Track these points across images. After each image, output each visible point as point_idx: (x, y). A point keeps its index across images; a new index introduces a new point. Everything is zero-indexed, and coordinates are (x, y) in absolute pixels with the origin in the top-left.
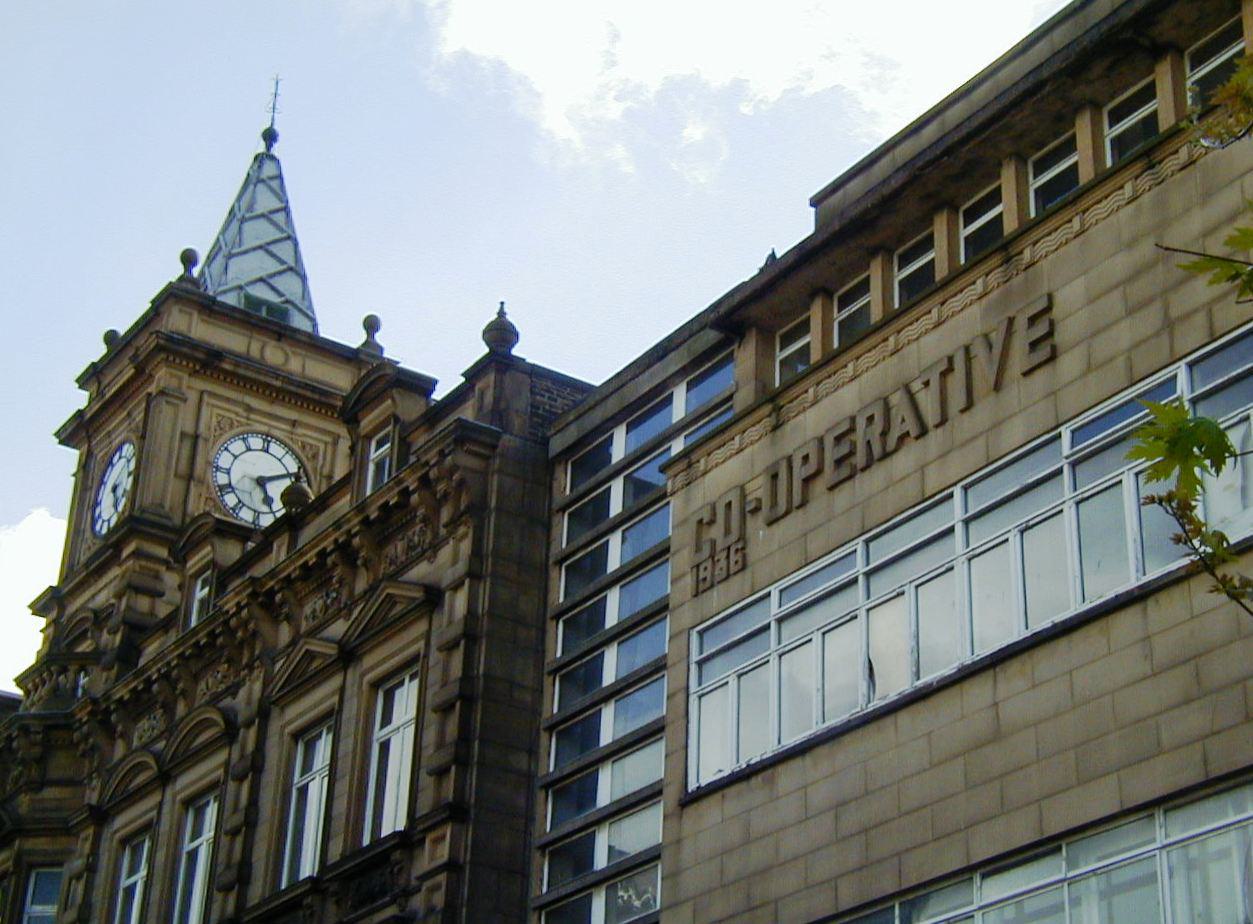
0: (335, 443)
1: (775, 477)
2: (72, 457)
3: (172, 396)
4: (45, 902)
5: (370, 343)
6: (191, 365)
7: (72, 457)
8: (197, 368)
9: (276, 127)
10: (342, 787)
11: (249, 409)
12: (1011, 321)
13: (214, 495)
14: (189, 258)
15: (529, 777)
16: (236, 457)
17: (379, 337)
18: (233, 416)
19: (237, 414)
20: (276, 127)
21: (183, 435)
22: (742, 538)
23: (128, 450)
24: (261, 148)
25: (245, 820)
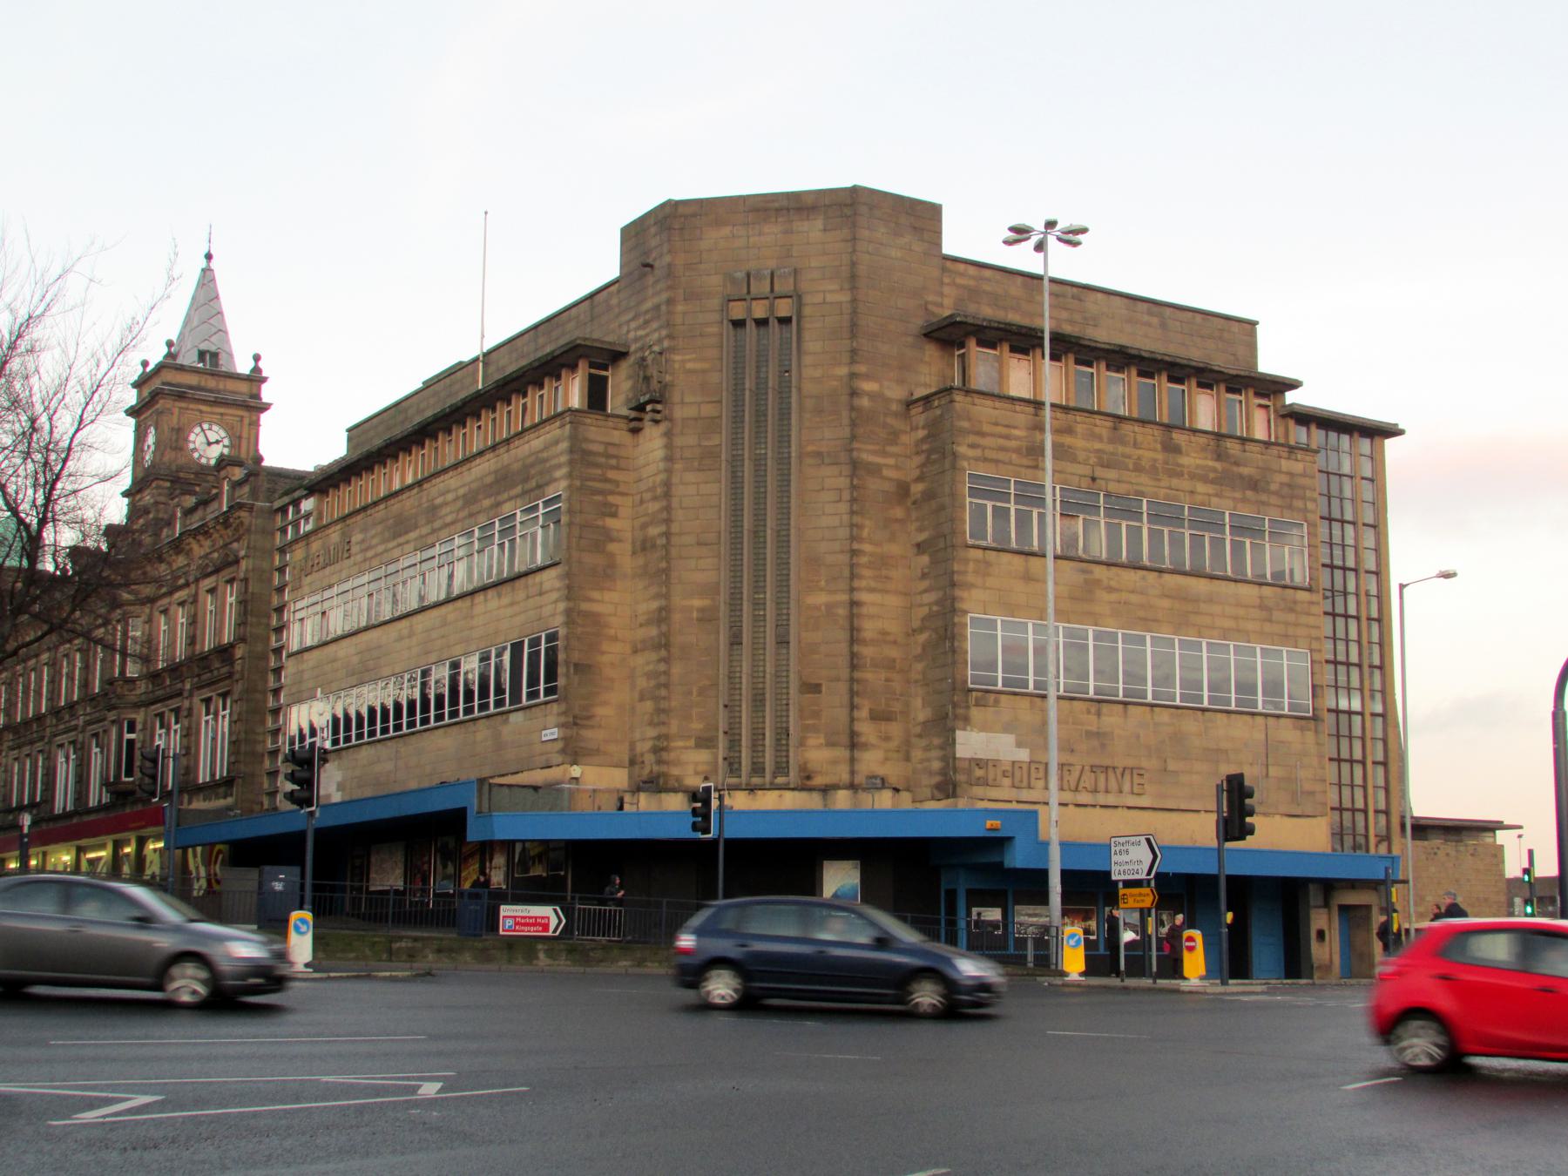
0: (242, 421)
4: (136, 631)
5: (257, 370)
9: (212, 252)
10: (218, 617)
11: (201, 412)
15: (268, 625)
21: (173, 429)
23: (152, 430)
25: (821, 793)
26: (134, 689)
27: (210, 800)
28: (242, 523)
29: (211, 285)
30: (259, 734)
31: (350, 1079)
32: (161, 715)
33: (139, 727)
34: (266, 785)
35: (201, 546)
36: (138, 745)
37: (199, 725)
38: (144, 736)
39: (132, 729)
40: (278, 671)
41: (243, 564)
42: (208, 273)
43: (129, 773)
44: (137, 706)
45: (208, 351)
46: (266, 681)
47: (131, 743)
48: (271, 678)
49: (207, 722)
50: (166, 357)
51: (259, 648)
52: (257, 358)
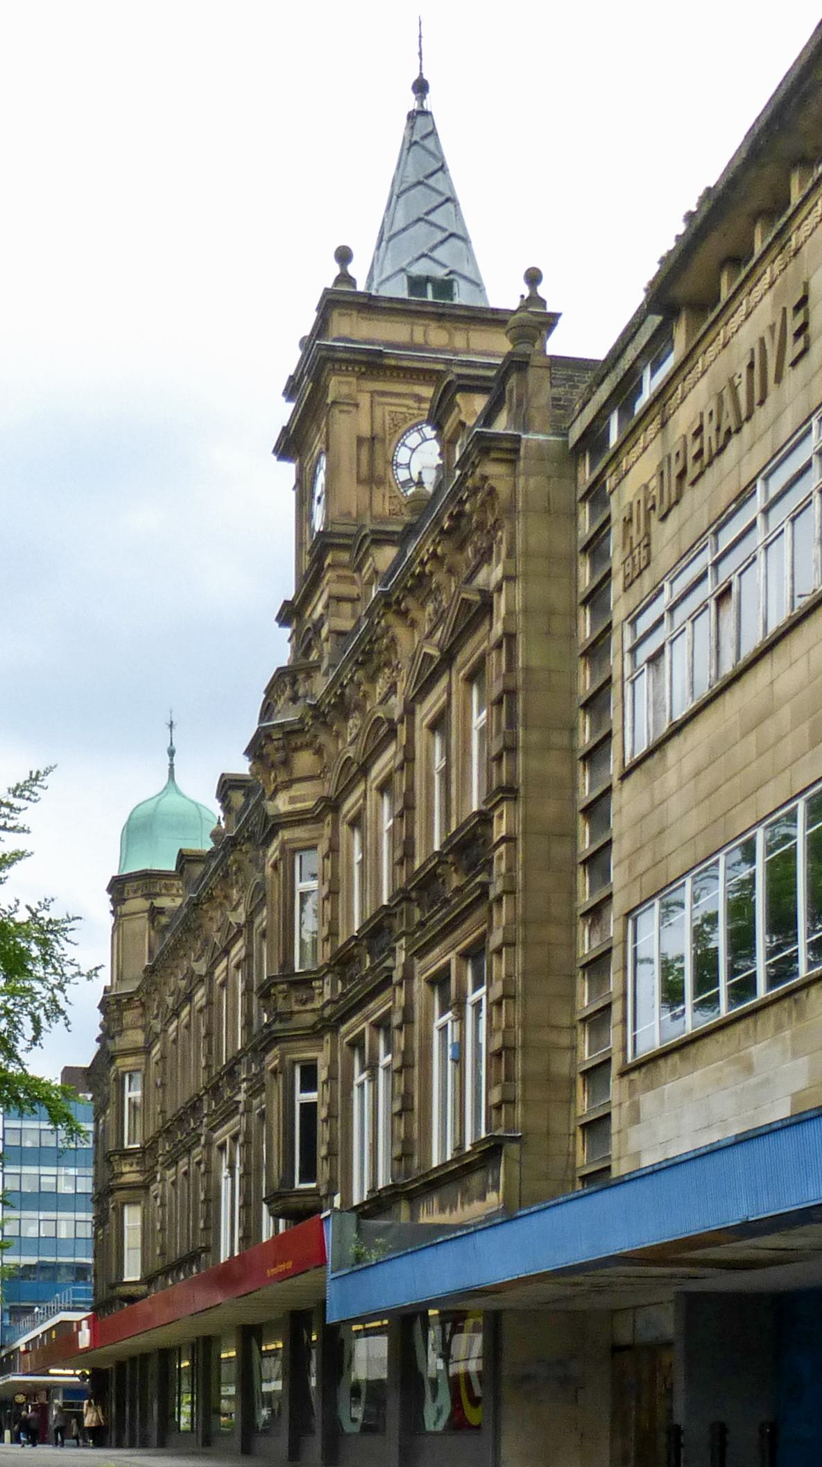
1: (662, 474)
2: (288, 470)
3: (343, 403)
5: (534, 300)
6: (357, 369)
7: (288, 470)
8: (363, 370)
12: (785, 309)
13: (397, 493)
14: (344, 256)
16: (413, 450)
17: (542, 290)
18: (404, 410)
19: (408, 407)
20: (425, 77)
21: (360, 441)
22: (647, 535)
24: (411, 103)
26: (311, 999)
27: (453, 1207)
28: (492, 492)
29: (429, 143)
30: (557, 1028)
31: (494, 802)
32: (356, 1044)
33: (322, 1075)
34: (581, 1157)
35: (413, 624)
36: (322, 1113)
37: (427, 1037)
38: (408, 1126)
39: (309, 1083)
40: (597, 810)
41: (501, 605)
42: (420, 120)
43: (309, 1173)
44: (315, 1033)
45: (428, 279)
46: (573, 893)
47: (309, 1110)
48: (584, 882)
49: (444, 1029)
50: (338, 280)
51: (551, 809)
52: (533, 277)
